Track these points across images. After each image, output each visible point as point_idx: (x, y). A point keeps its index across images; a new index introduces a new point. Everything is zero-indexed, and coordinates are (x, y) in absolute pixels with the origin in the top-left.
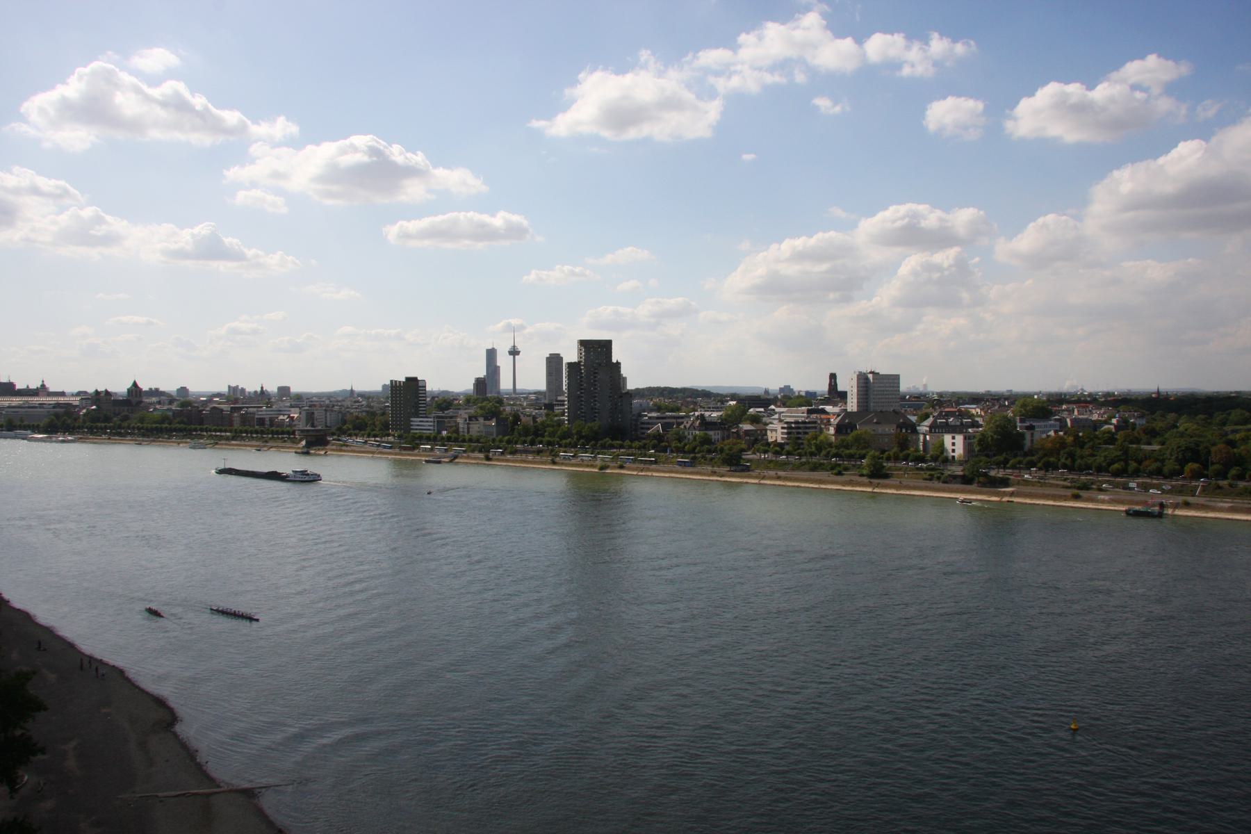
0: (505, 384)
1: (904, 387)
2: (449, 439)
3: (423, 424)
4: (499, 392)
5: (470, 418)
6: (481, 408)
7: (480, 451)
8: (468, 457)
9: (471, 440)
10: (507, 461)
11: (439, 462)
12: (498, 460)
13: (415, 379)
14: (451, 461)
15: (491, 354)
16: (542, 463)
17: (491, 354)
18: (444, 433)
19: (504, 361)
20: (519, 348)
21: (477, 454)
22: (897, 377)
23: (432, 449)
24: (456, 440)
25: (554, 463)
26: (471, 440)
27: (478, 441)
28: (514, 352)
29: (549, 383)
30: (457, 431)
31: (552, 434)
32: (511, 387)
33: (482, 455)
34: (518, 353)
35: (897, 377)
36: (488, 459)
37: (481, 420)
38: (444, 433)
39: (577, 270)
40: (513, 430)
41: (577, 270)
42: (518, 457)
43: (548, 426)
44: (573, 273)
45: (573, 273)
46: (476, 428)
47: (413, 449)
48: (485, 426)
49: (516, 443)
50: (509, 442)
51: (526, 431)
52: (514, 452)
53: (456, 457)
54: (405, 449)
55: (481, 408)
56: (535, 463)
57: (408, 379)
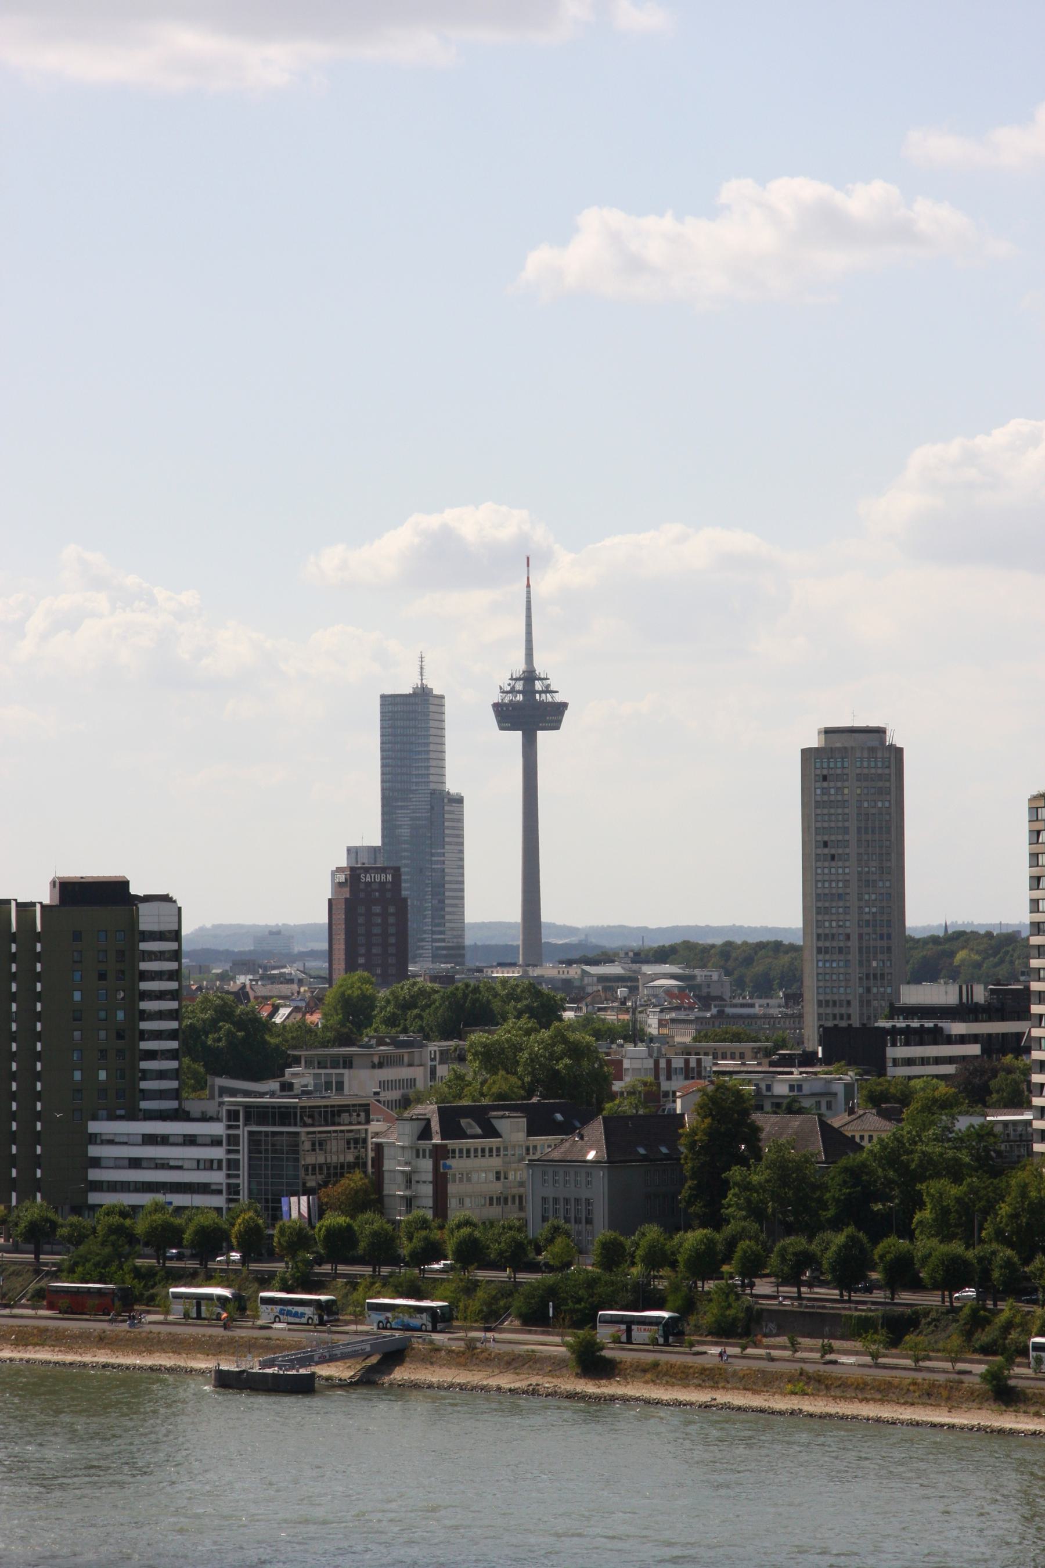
0: (488, 899)
1: (348, 896)
2: (340, 1246)
3: (166, 1156)
4: (456, 952)
5: (451, 1121)
6: (493, 1059)
7: (535, 1319)
8: (471, 1356)
9: (471, 1254)
10: (711, 1377)
11: (305, 1387)
12: (654, 1372)
13: (112, 894)
14: (368, 1381)
15: (410, 726)
16: (930, 1394)
17: (410, 726)
18: (298, 1207)
19: (477, 763)
20: (561, 681)
21: (512, 1337)
22: (805, 752)
23: (240, 1306)
24: (382, 1251)
25: (1004, 1394)
26: (471, 1254)
27: (518, 1257)
28: (529, 712)
29: (820, 898)
30: (372, 1198)
31: (960, 1221)
32: (513, 913)
33: (553, 1345)
34: (552, 715)
35: (805, 752)
36: (592, 1363)
37: (513, 1129)
38: (298, 1207)
39: (864, 200)
40: (712, 1189)
41: (864, 200)
42: (774, 1352)
43: (931, 1168)
44: (828, 225)
45: (828, 225)
46: (487, 1177)
47: (126, 1303)
48: (541, 1166)
49: (752, 1269)
50: (706, 1263)
51: (796, 1203)
52: (743, 1326)
53: (394, 1356)
54: (74, 1305)
55: (493, 1059)
56: (885, 1392)
57: (74, 893)
